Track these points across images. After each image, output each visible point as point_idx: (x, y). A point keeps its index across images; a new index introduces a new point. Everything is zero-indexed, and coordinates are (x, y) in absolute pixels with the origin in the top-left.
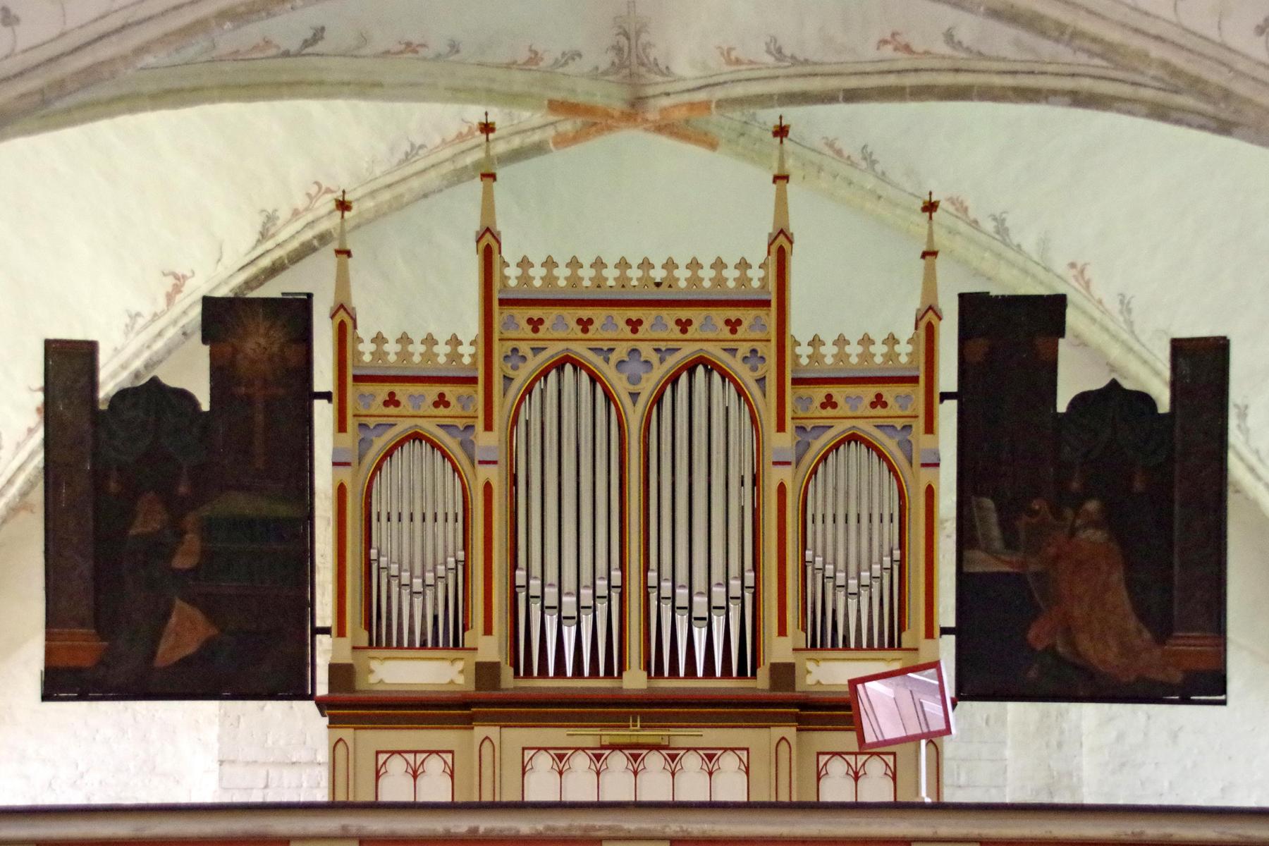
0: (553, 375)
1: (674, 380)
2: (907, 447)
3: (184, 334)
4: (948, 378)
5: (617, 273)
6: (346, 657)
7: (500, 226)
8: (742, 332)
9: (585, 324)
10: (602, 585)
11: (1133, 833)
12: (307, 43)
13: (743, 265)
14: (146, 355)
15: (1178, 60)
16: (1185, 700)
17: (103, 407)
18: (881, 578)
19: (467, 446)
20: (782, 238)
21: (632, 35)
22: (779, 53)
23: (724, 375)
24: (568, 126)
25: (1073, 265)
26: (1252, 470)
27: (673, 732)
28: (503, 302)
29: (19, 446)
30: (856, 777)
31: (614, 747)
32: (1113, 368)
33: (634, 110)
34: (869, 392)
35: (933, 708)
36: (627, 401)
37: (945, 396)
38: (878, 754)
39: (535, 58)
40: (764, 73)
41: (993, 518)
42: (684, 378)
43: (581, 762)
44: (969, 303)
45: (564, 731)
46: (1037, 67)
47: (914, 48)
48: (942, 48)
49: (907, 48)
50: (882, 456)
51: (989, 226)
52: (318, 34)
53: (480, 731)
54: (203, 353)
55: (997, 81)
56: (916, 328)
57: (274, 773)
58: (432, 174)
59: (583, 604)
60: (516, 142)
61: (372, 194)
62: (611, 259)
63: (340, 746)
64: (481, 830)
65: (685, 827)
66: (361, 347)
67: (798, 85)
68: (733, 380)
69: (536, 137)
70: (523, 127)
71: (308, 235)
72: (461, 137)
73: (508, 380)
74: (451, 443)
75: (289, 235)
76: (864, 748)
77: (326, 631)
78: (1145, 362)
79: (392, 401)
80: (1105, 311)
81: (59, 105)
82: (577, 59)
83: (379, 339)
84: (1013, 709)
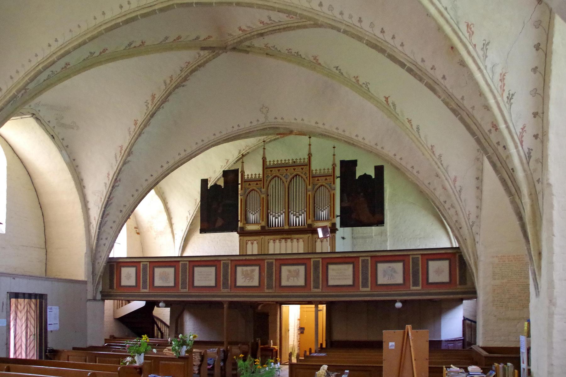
4: (338, 173)
8: (304, 170)
19: (261, 191)
36: (285, 182)
42: (295, 177)
43: (277, 241)
44: (342, 162)
54: (222, 179)
73: (267, 180)
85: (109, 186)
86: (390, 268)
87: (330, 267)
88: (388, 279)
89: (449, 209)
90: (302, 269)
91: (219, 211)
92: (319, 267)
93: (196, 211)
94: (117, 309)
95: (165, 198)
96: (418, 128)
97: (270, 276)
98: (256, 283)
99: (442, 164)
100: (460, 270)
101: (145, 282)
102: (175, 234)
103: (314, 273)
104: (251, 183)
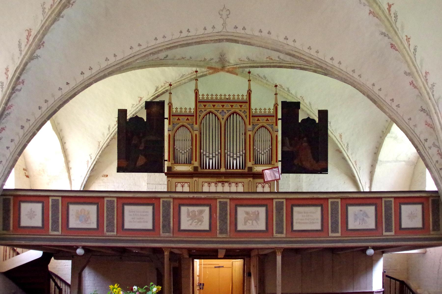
0: (208, 115)
1: (230, 116)
2: (272, 128)
3: (142, 108)
4: (280, 116)
5: (220, 97)
6: (170, 165)
7: (199, 88)
9: (214, 106)
10: (217, 152)
12: (165, 58)
13: (243, 95)
14: (135, 111)
15: (318, 63)
16: (321, 173)
17: (128, 121)
18: (268, 152)
20: (250, 91)
22: (249, 59)
23: (239, 115)
24: (211, 71)
25: (301, 97)
26: (332, 133)
27: (230, 179)
28: (199, 102)
29: (113, 128)
30: (263, 187)
31: (219, 182)
32: (308, 114)
33: (223, 68)
34: (266, 118)
35: (277, 175)
36: (222, 119)
37: (279, 119)
38: (267, 183)
40: (247, 62)
43: (213, 184)
44: (283, 103)
45: (210, 179)
46: (294, 63)
47: (273, 59)
48: (277, 59)
49: (271, 59)
50: (268, 130)
51: (286, 89)
52: (167, 56)
53: (194, 179)
55: (287, 65)
56: (274, 107)
57: (157, 186)
58: (186, 79)
59: (213, 156)
60: (201, 74)
61: (175, 83)
62: (219, 94)
63: (169, 181)
64: (195, 196)
66: (173, 110)
67: (252, 65)
68: (241, 116)
69: (205, 73)
71: (164, 90)
72: (192, 73)
73: (200, 116)
74: (189, 127)
75: (161, 90)
76: (265, 182)
77: (166, 160)
78: (314, 114)
79: (179, 119)
80: (307, 105)
81: (122, 69)
83: (176, 108)
84: (291, 175)
85: (7, 87)
86: (362, 212)
87: (296, 209)
88: (360, 224)
89: (430, 148)
90: (262, 211)
91: (141, 148)
92: (283, 209)
93: (99, 155)
94: (3, 260)
95: (63, 137)
96: (415, 50)
97: (223, 219)
98: (205, 226)
99: (433, 95)
100: (433, 216)
101: (55, 222)
102: (72, 180)
104: (181, 118)
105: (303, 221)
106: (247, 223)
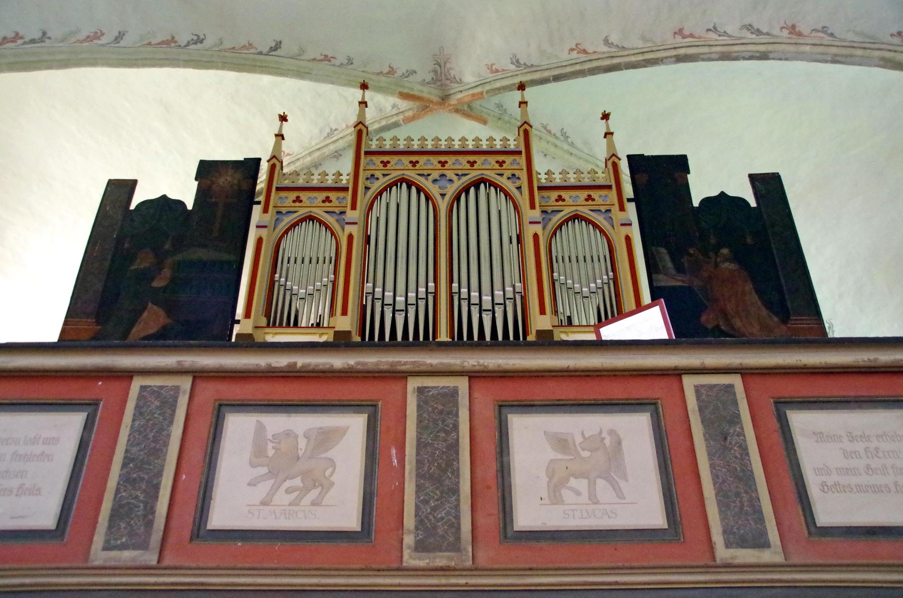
1: (466, 190)
4: (628, 190)
11: (869, 359)
21: (443, 65)
22: (517, 63)
28: (367, 153)
36: (439, 198)
39: (392, 71)
41: (667, 258)
46: (655, 49)
49: (585, 52)
64: (299, 364)
65: (481, 361)
69: (393, 120)
70: (388, 115)
82: (414, 74)
92: (736, 419)
103: (711, 455)
105: (854, 480)
106: (566, 494)
